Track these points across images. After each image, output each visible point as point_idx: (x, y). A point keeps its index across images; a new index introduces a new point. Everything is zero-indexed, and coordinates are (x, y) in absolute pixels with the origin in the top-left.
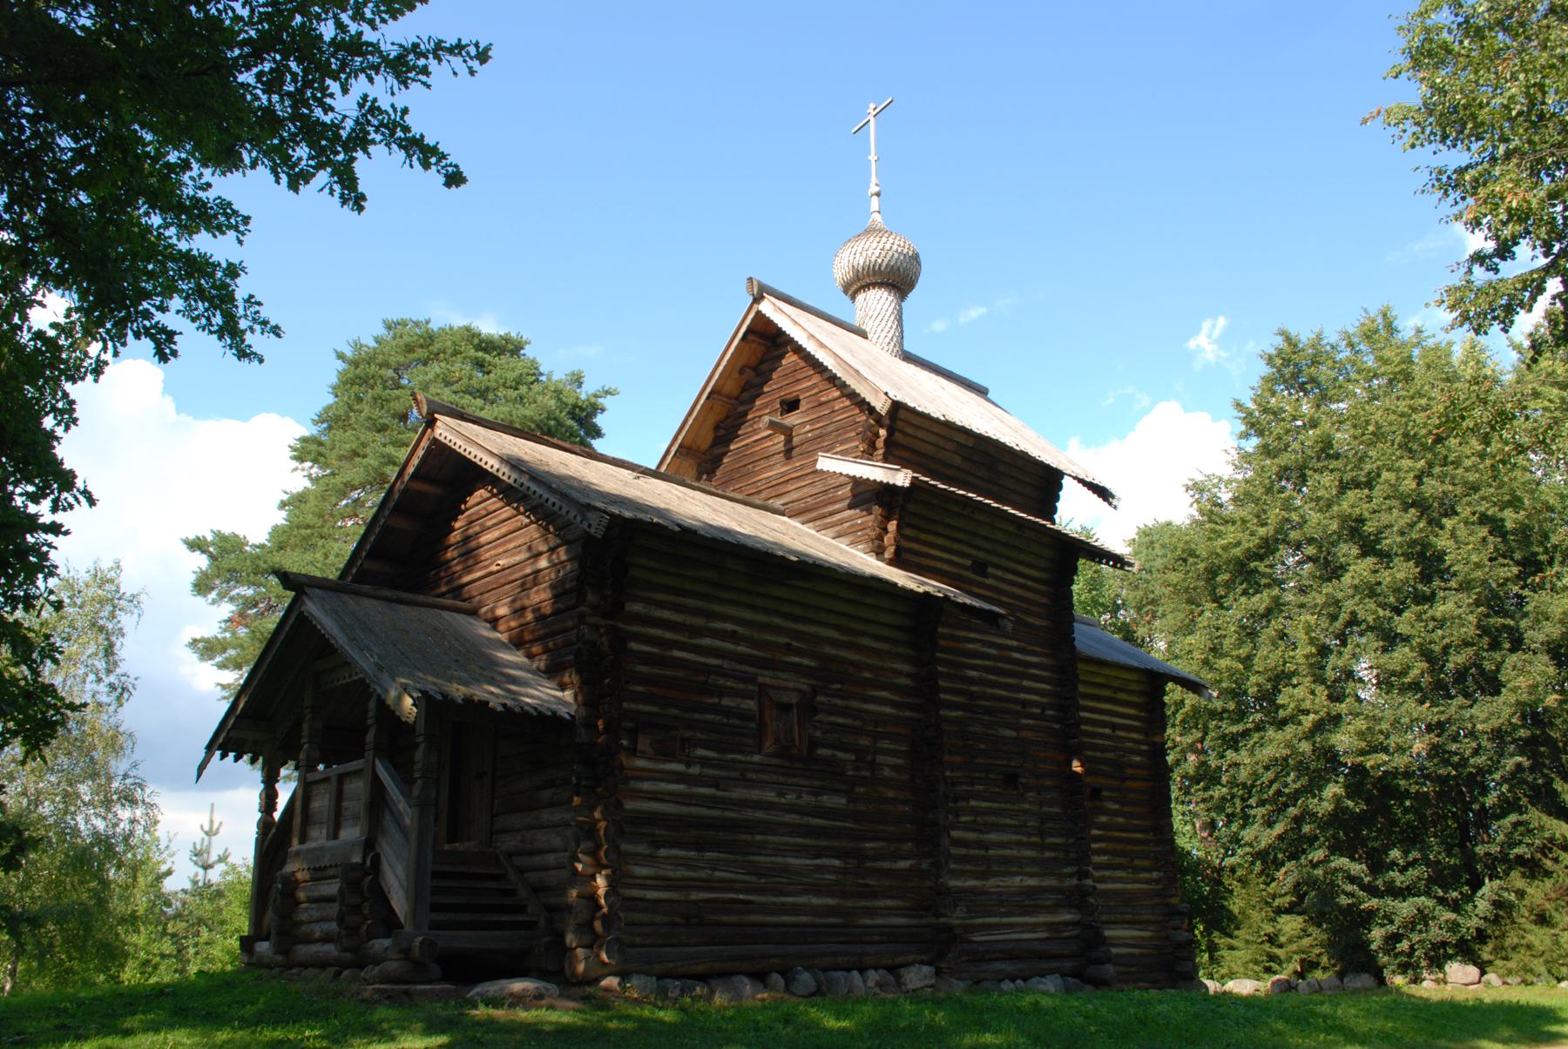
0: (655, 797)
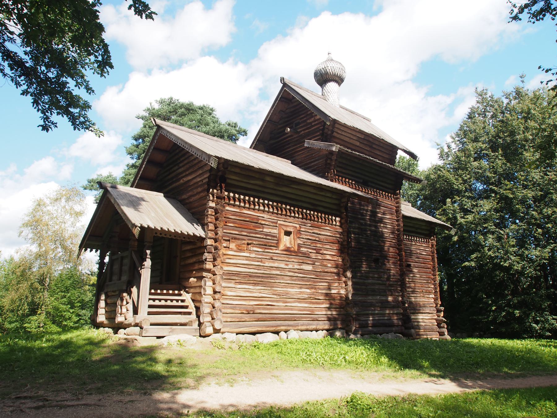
0: (235, 265)
